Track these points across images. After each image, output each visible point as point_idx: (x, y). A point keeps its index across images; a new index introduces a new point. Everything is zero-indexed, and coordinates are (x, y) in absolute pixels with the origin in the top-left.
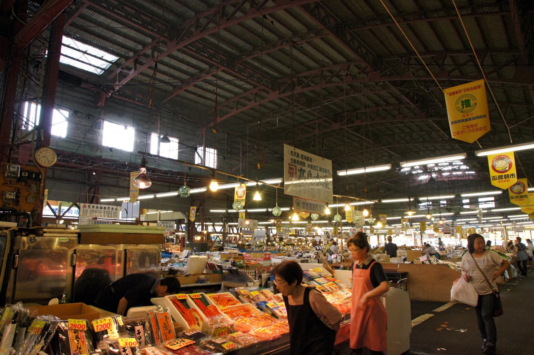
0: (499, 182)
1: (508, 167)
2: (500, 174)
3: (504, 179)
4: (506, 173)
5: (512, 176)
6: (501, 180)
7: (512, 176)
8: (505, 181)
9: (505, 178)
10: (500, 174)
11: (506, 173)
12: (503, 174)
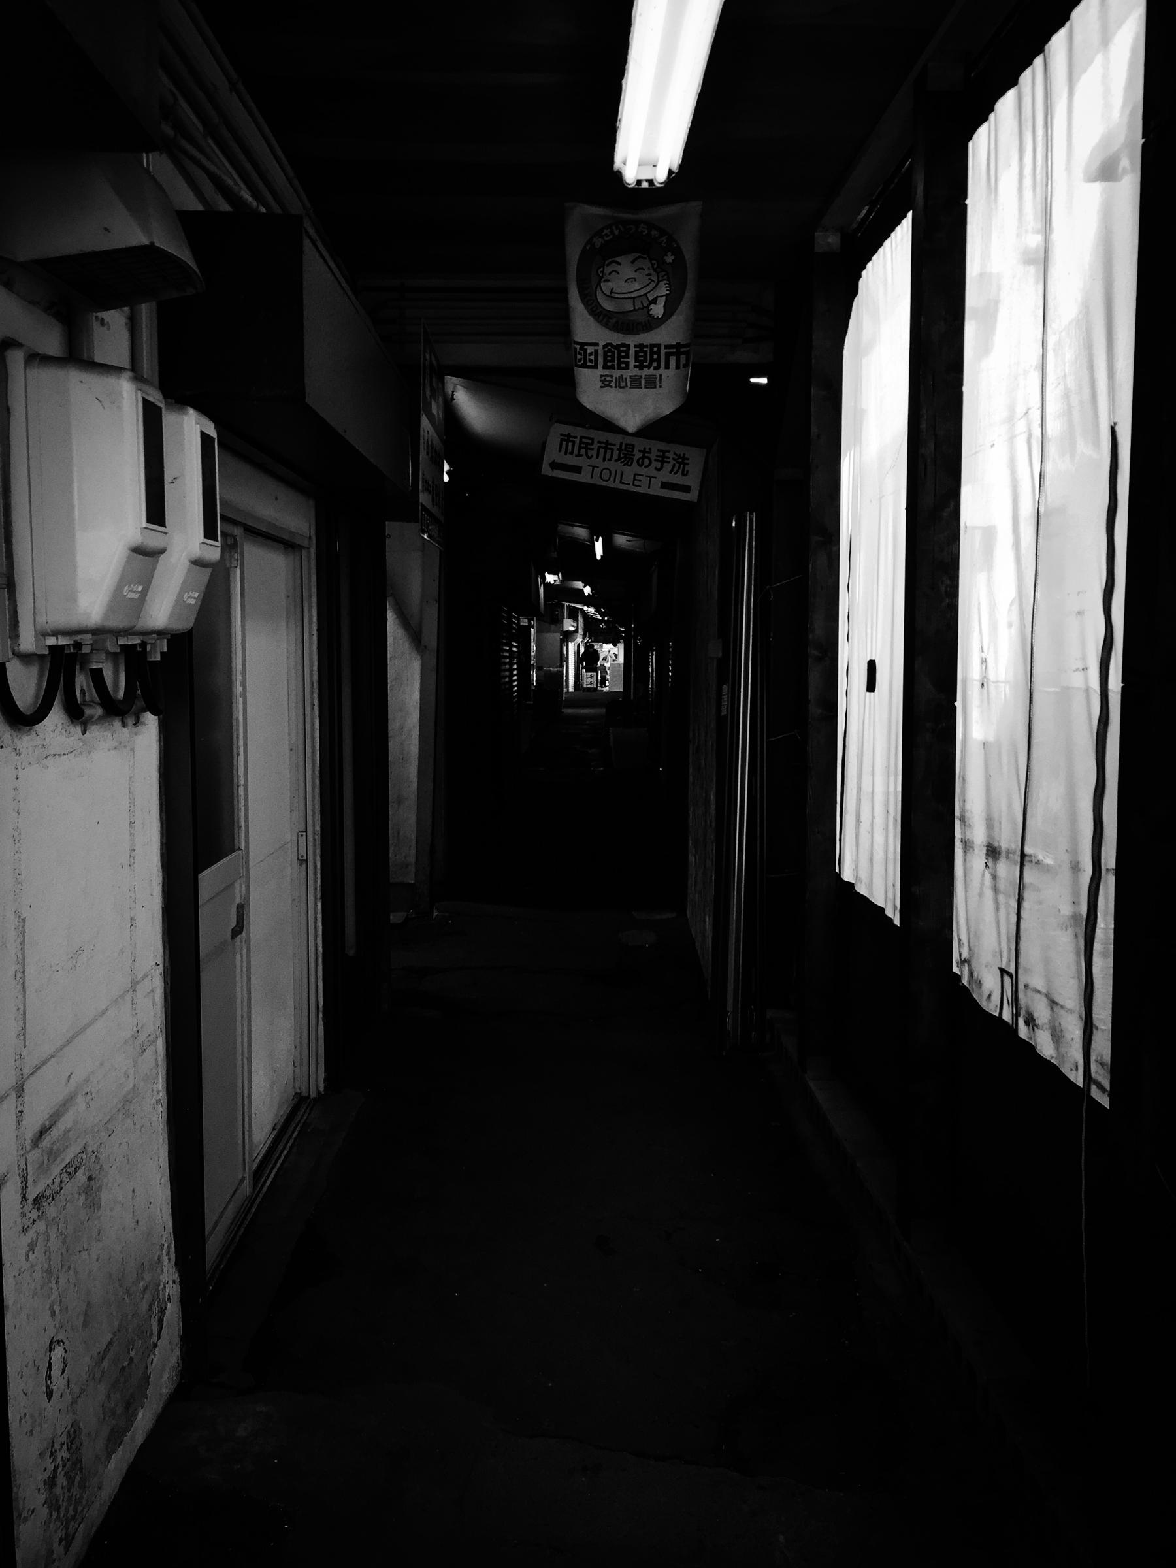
0: (605, 383)
1: (661, 302)
2: (616, 338)
3: (633, 371)
4: (647, 338)
5: (606, 449)
6: (617, 373)
7: (606, 449)
8: (636, 383)
9: (641, 367)
10: (616, 338)
11: (647, 338)
12: (632, 341)
